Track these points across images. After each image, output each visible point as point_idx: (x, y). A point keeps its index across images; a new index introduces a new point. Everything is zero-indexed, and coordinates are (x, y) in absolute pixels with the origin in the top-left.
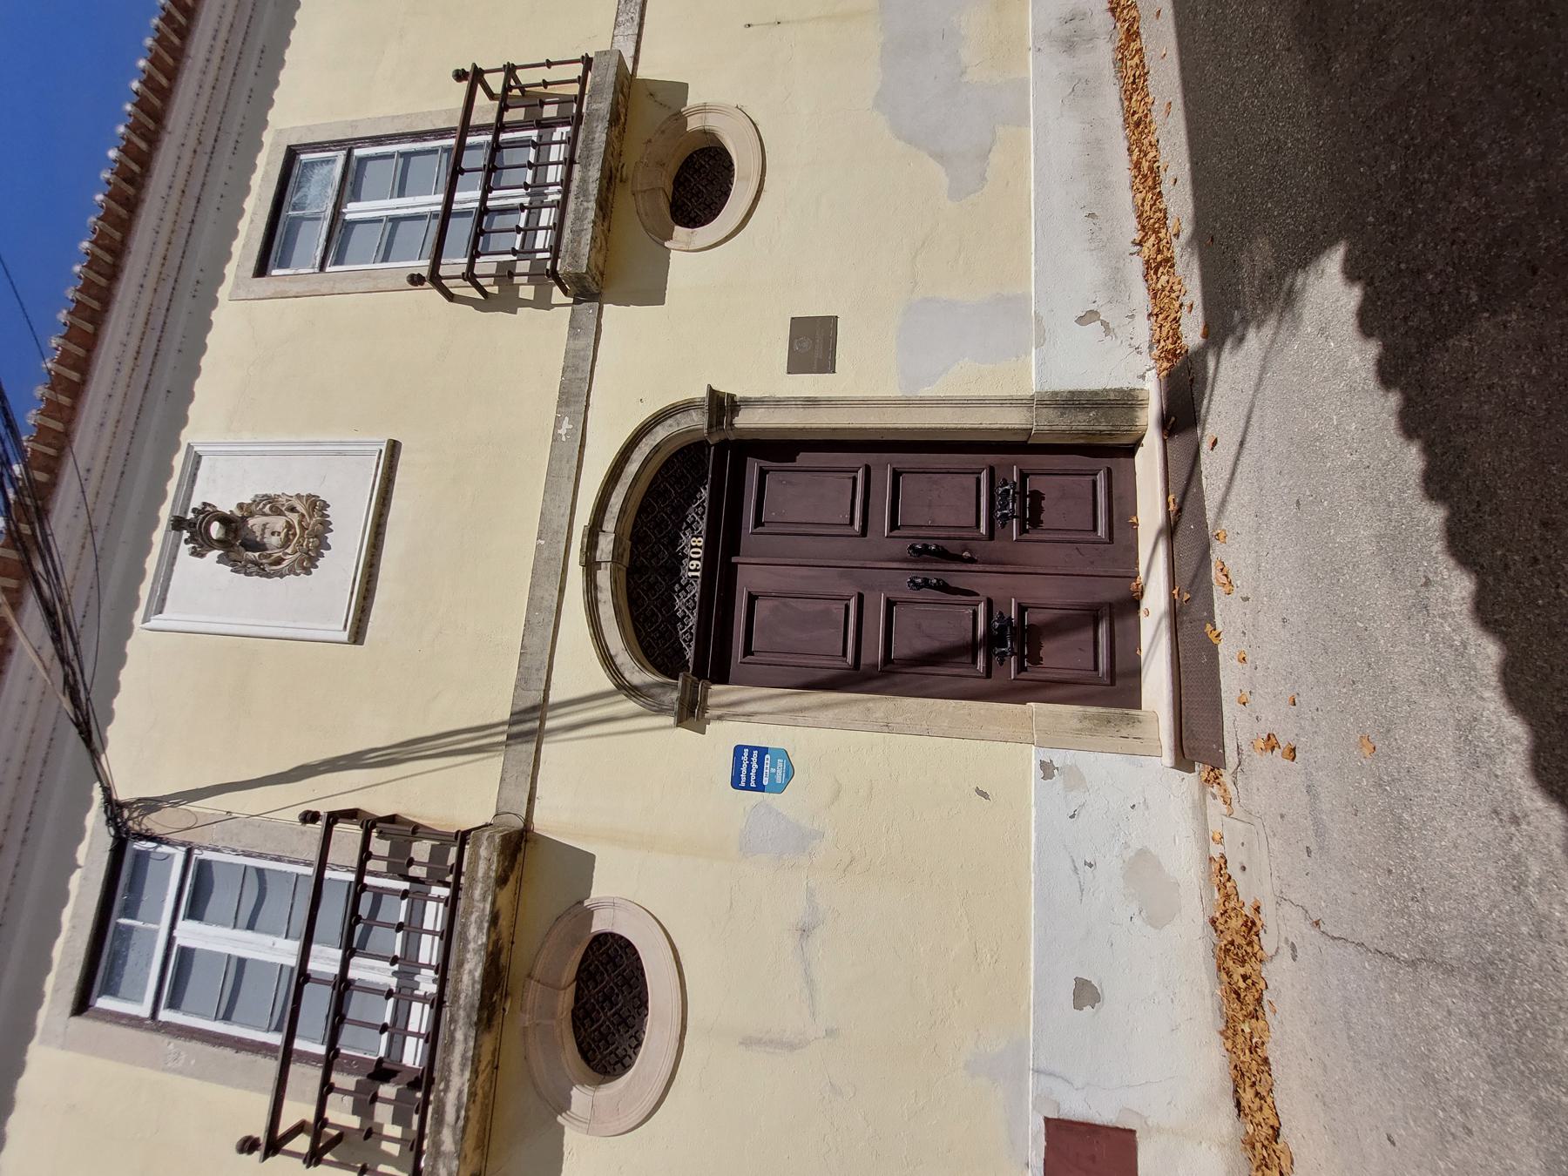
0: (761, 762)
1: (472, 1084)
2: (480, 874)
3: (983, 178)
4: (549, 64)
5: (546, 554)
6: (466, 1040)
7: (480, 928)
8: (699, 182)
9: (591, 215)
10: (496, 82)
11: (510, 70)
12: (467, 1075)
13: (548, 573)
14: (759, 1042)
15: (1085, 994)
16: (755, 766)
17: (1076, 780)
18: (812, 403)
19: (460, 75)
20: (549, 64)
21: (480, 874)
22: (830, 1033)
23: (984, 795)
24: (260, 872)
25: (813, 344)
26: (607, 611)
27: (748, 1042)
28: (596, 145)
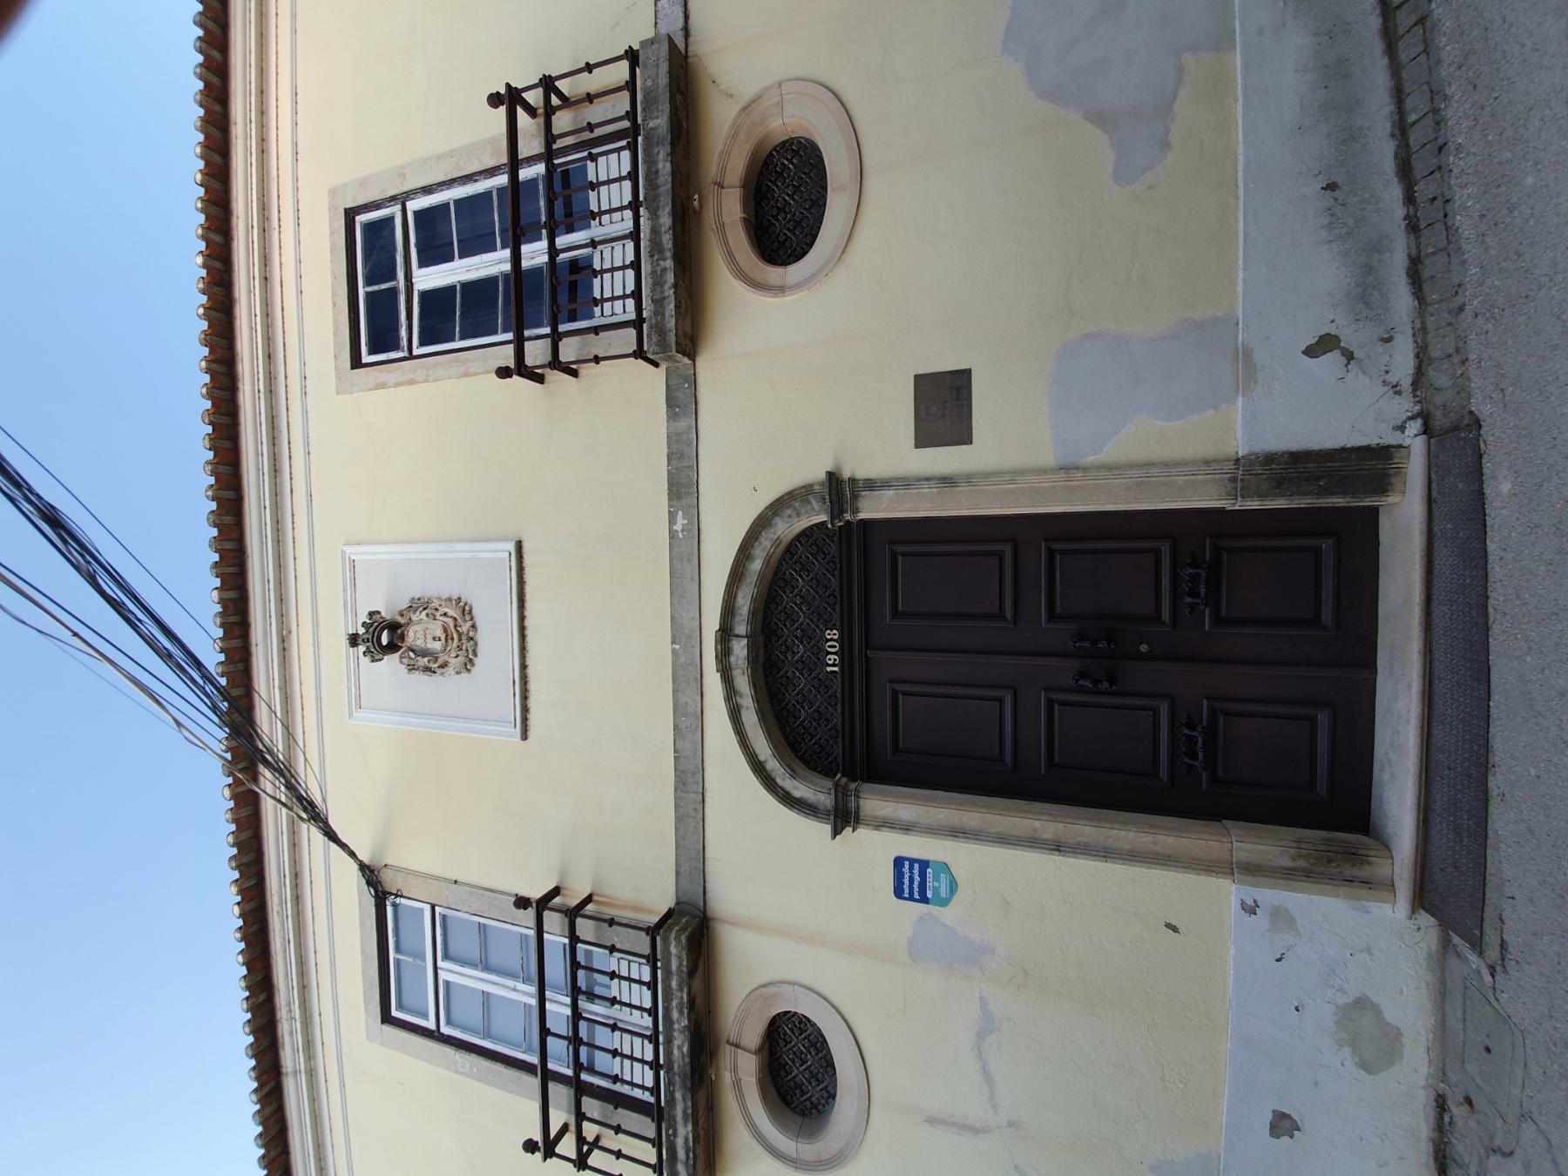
0: (923, 875)
1: (695, 1131)
2: (674, 968)
3: (1166, 145)
4: (589, 68)
5: (682, 659)
6: (684, 1100)
7: (681, 1013)
8: (787, 203)
9: (670, 278)
10: (534, 97)
11: (548, 84)
12: (690, 1127)
13: (686, 679)
14: (943, 1122)
15: (1282, 1125)
16: (917, 879)
17: (1282, 920)
18: (947, 481)
19: (495, 100)
20: (589, 68)
21: (674, 968)
22: (1011, 1124)
23: (1174, 929)
24: (486, 995)
25: (944, 405)
26: (750, 718)
27: (932, 1121)
28: (661, 180)
